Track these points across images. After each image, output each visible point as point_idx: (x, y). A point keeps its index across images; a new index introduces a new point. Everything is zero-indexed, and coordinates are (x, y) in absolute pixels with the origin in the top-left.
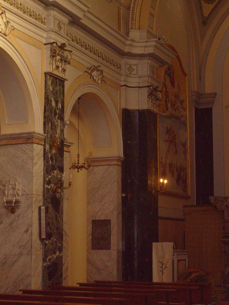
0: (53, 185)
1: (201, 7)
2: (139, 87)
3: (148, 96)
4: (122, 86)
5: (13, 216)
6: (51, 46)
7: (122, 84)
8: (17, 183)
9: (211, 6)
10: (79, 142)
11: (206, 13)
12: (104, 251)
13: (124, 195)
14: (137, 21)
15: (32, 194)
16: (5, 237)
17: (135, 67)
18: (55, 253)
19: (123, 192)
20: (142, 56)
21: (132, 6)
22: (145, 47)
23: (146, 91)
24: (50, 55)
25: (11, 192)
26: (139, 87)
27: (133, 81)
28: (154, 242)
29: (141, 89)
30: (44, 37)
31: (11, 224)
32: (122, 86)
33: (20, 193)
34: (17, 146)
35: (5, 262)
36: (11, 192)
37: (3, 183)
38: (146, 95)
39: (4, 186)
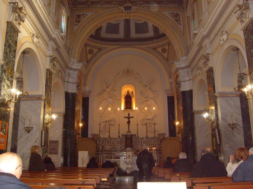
0: (47, 121)
1: (87, 56)
2: (73, 83)
3: (76, 87)
4: (66, 81)
5: (28, 134)
6: (51, 58)
7: (66, 81)
8: (32, 119)
9: (91, 56)
10: (239, 62)
11: (89, 58)
12: (55, 155)
13: (64, 130)
14: (73, 55)
15: (40, 124)
16: (23, 145)
17: (71, 74)
18: (46, 153)
19: (64, 129)
20: (75, 70)
21: (71, 49)
22: (77, 66)
23: (75, 85)
24: (49, 61)
25: (28, 123)
26: (73, 83)
27: (71, 80)
28: (80, 151)
29: (73, 84)
30: (50, 53)
31: (27, 138)
32: (66, 81)
33: (33, 123)
34: (33, 101)
35: (23, 157)
36: (28, 123)
37: (24, 118)
38: (76, 86)
39: (25, 120)
